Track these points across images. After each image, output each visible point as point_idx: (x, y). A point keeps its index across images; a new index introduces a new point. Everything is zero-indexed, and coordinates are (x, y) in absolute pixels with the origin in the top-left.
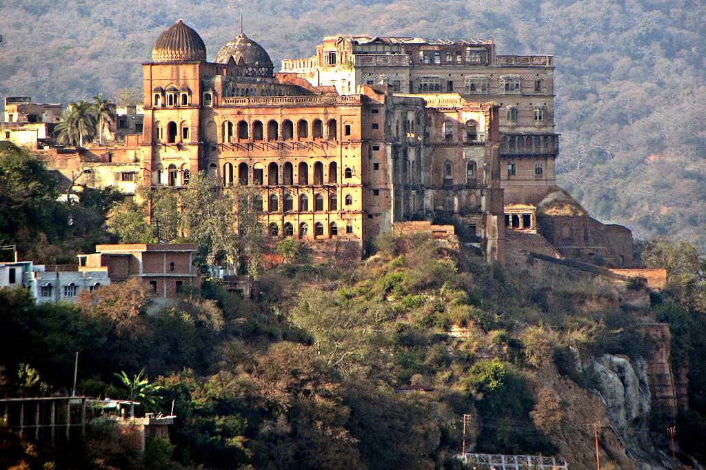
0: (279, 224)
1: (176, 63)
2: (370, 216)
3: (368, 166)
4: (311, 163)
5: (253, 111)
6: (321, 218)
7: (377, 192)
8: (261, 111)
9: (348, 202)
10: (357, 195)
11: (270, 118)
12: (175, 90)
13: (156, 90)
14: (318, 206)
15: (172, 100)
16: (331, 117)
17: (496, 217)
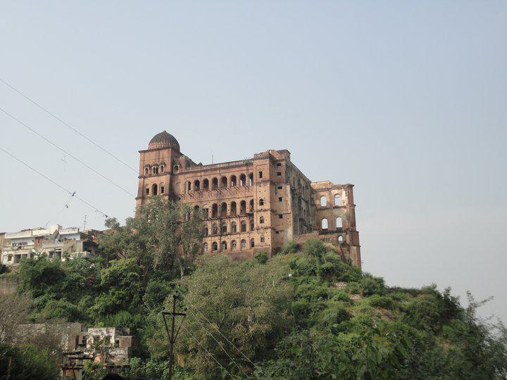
0: (218, 242)
1: (159, 149)
2: (277, 232)
3: (276, 199)
4: (238, 202)
5: (203, 173)
6: (244, 236)
7: (281, 216)
8: (207, 173)
9: (262, 221)
10: (267, 216)
11: (213, 176)
12: (157, 165)
13: (146, 166)
14: (243, 228)
15: (156, 171)
16: (251, 171)
17: (355, 247)
